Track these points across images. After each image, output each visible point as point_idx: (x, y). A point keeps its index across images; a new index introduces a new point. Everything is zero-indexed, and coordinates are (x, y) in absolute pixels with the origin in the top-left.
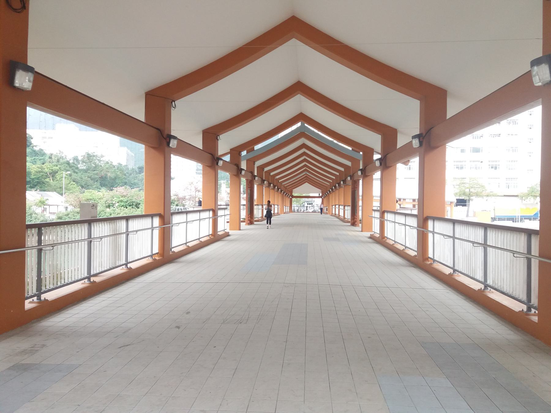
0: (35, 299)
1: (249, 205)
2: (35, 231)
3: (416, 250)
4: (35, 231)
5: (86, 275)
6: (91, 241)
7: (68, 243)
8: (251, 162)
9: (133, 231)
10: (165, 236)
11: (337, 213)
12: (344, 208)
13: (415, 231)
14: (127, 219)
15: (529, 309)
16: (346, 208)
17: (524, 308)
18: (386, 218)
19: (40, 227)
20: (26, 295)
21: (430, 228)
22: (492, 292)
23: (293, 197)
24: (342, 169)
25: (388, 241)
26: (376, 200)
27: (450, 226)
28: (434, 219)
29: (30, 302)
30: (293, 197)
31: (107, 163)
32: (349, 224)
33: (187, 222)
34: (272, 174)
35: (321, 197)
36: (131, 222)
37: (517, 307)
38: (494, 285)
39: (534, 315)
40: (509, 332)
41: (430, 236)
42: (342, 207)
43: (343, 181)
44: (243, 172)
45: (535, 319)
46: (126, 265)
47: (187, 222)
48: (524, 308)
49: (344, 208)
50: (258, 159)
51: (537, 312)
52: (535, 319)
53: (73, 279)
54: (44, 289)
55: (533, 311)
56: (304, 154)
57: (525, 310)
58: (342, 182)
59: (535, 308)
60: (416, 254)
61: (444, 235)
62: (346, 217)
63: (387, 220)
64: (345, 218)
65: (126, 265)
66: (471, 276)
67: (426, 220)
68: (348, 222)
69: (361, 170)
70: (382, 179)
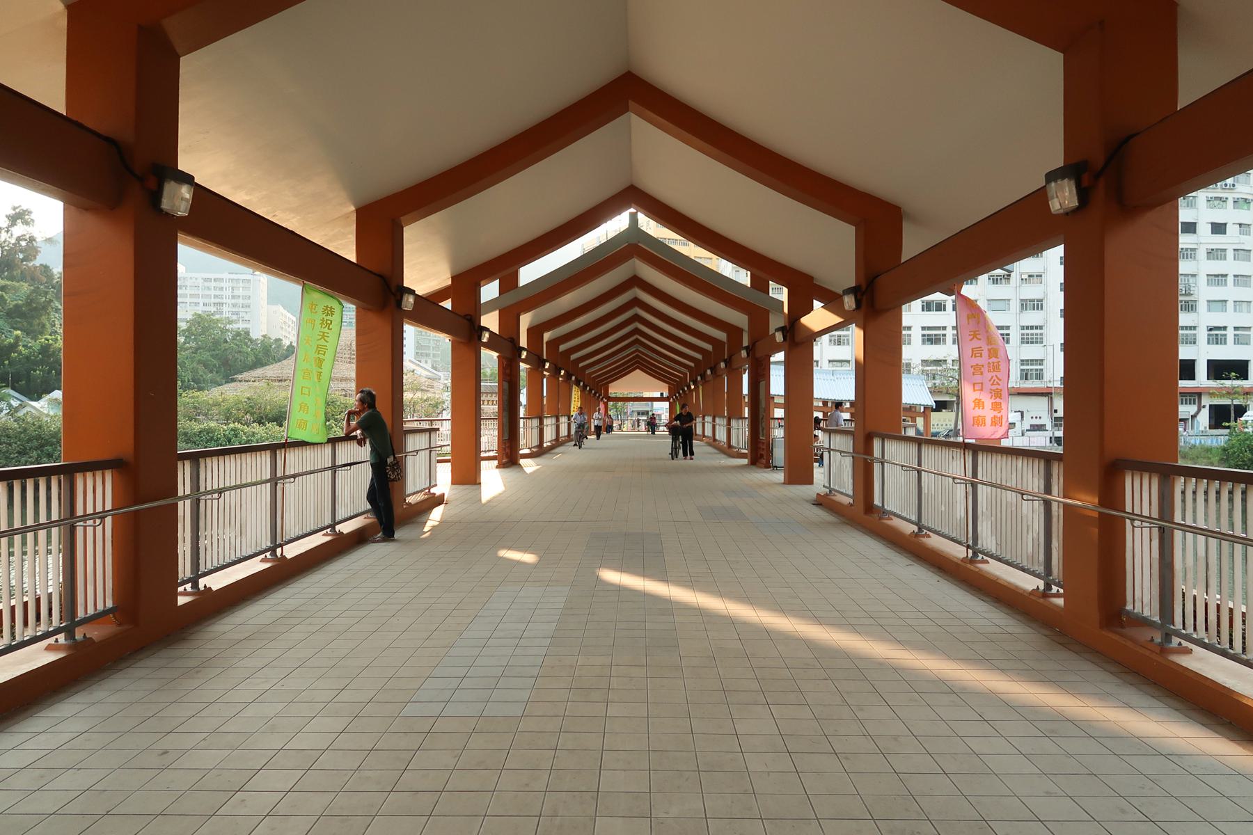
0: (61, 638)
1: (506, 420)
2: (188, 464)
3: (851, 493)
4: (188, 464)
5: (269, 544)
6: (198, 500)
7: (294, 476)
8: (509, 318)
9: (212, 492)
10: (147, 542)
11: (708, 432)
12: (729, 423)
13: (848, 461)
14: (273, 448)
15: (1048, 587)
16: (717, 420)
17: (1041, 584)
18: (1178, 518)
19: (195, 458)
20: (181, 576)
21: (877, 452)
22: (1190, 651)
23: (610, 399)
24: (709, 347)
25: (896, 522)
26: (778, 406)
27: (913, 449)
28: (883, 438)
29: (262, 561)
30: (610, 399)
31: (238, 334)
32: (745, 461)
33: (334, 468)
34: (573, 357)
35: (667, 399)
36: (280, 454)
37: (1030, 584)
38: (1019, 561)
39: (1057, 595)
40: (1011, 622)
41: (877, 467)
42: (708, 419)
43: (725, 361)
44: (524, 354)
45: (1060, 602)
46: (332, 526)
47: (334, 468)
48: (1041, 584)
49: (729, 423)
50: (563, 343)
51: (1061, 591)
52: (1060, 602)
53: (233, 558)
54: (202, 569)
55: (1055, 589)
56: (637, 341)
57: (1042, 588)
58: (709, 372)
59: (1058, 585)
60: (851, 501)
61: (841, 452)
62: (734, 443)
63: (1186, 528)
64: (730, 446)
65: (332, 526)
66: (1008, 557)
67: (869, 439)
68: (743, 456)
69: (747, 348)
70: (787, 364)
